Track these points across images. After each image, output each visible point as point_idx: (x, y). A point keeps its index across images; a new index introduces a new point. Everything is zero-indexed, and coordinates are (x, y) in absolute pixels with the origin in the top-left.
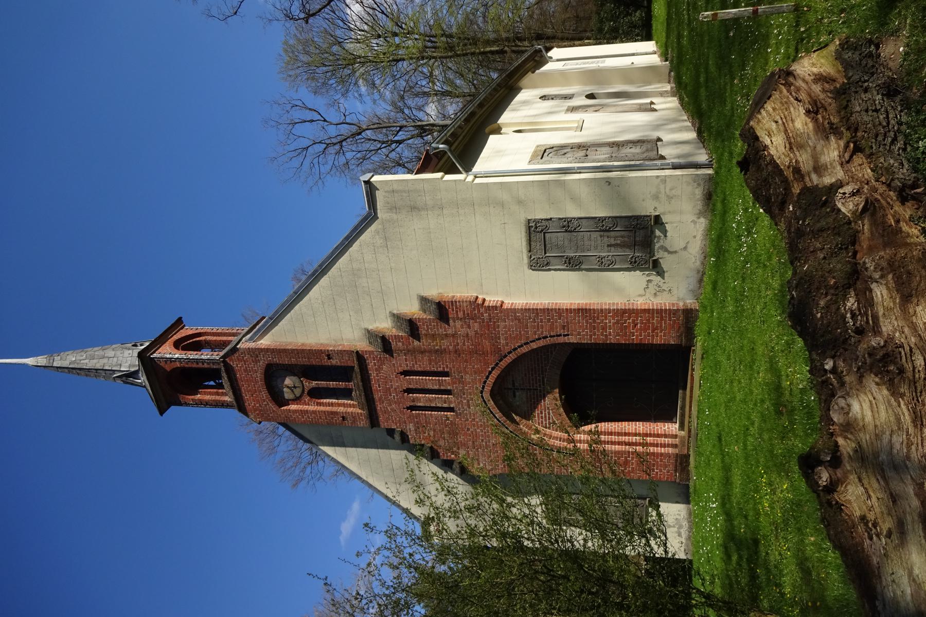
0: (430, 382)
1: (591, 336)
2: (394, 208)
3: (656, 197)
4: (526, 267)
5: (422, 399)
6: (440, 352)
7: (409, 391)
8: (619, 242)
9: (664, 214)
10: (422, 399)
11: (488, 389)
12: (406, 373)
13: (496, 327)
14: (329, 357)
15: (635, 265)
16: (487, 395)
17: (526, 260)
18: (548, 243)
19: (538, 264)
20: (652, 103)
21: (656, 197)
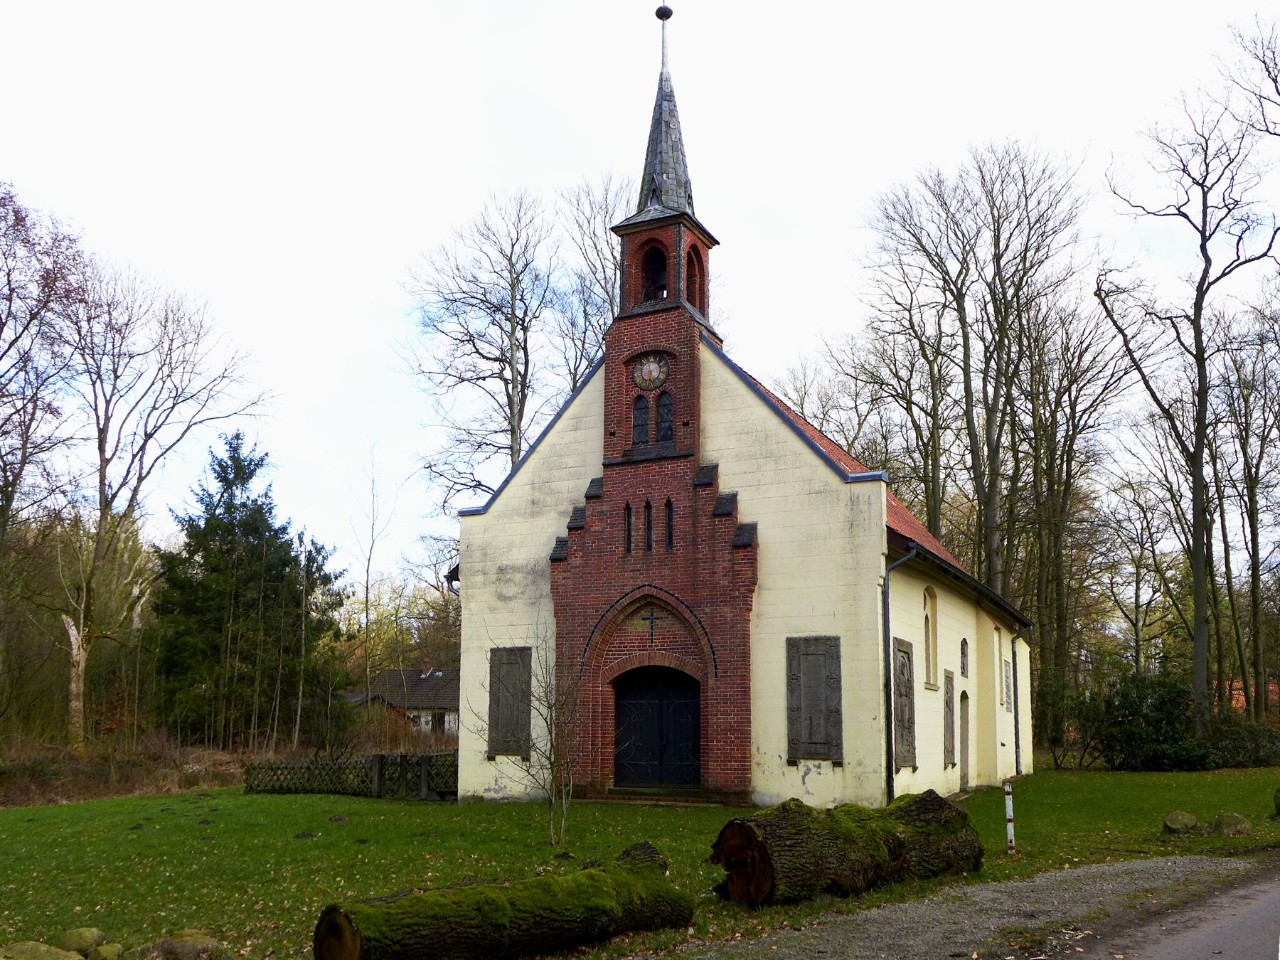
0: (658, 533)
5: (638, 522)
7: (648, 506)
10: (638, 522)
11: (654, 592)
12: (669, 504)
13: (725, 603)
16: (646, 590)
17: (795, 635)
18: (814, 661)
19: (795, 647)
20: (954, 765)
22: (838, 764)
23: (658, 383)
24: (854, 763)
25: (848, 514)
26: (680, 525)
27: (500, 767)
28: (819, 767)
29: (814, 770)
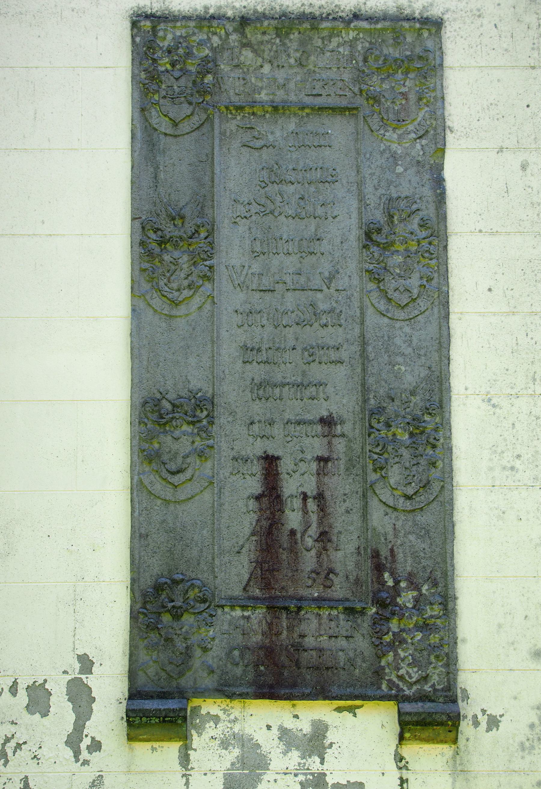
8: (293, 519)
9: (458, 769)
15: (160, 602)
28: (316, 743)
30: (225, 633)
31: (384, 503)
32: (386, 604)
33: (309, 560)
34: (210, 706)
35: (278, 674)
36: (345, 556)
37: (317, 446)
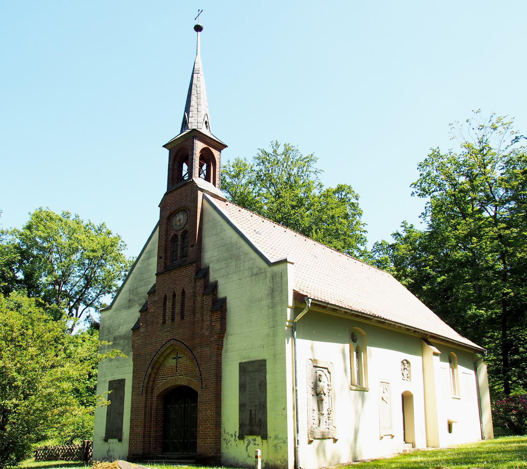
0: (178, 310)
1: (202, 402)
2: (273, 277)
3: (276, 438)
4: (240, 361)
5: (169, 304)
6: (194, 313)
8: (253, 416)
9: (267, 443)
10: (169, 304)
12: (183, 293)
14: (161, 258)
15: (242, 425)
17: (244, 361)
19: (244, 368)
21: (276, 438)
22: (265, 437)
23: (182, 226)
24: (272, 438)
25: (271, 285)
26: (188, 304)
27: (111, 445)
28: (255, 440)
29: (252, 442)
30: (247, 428)
31: (297, 400)
32: (260, 425)
33: (254, 421)
34: (246, 436)
35: (251, 433)
36: (257, 420)
37: (255, 408)
